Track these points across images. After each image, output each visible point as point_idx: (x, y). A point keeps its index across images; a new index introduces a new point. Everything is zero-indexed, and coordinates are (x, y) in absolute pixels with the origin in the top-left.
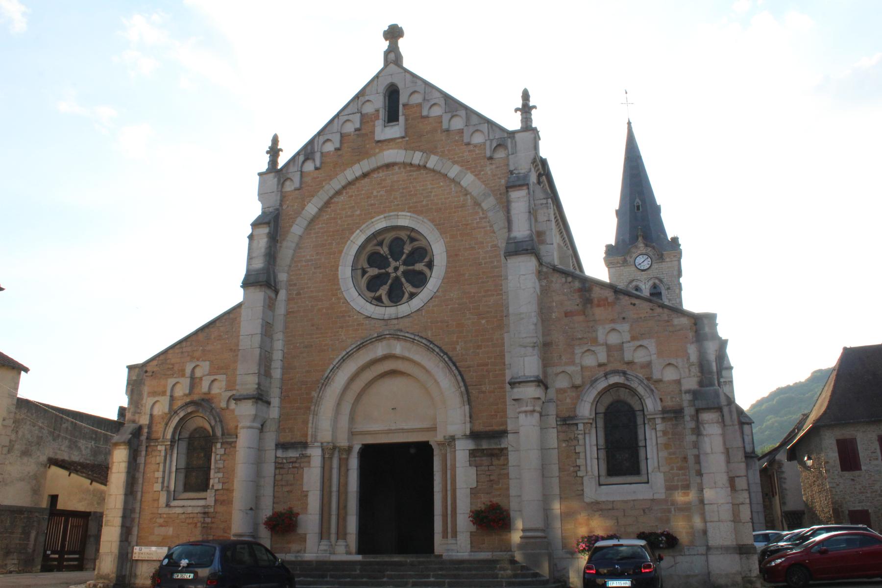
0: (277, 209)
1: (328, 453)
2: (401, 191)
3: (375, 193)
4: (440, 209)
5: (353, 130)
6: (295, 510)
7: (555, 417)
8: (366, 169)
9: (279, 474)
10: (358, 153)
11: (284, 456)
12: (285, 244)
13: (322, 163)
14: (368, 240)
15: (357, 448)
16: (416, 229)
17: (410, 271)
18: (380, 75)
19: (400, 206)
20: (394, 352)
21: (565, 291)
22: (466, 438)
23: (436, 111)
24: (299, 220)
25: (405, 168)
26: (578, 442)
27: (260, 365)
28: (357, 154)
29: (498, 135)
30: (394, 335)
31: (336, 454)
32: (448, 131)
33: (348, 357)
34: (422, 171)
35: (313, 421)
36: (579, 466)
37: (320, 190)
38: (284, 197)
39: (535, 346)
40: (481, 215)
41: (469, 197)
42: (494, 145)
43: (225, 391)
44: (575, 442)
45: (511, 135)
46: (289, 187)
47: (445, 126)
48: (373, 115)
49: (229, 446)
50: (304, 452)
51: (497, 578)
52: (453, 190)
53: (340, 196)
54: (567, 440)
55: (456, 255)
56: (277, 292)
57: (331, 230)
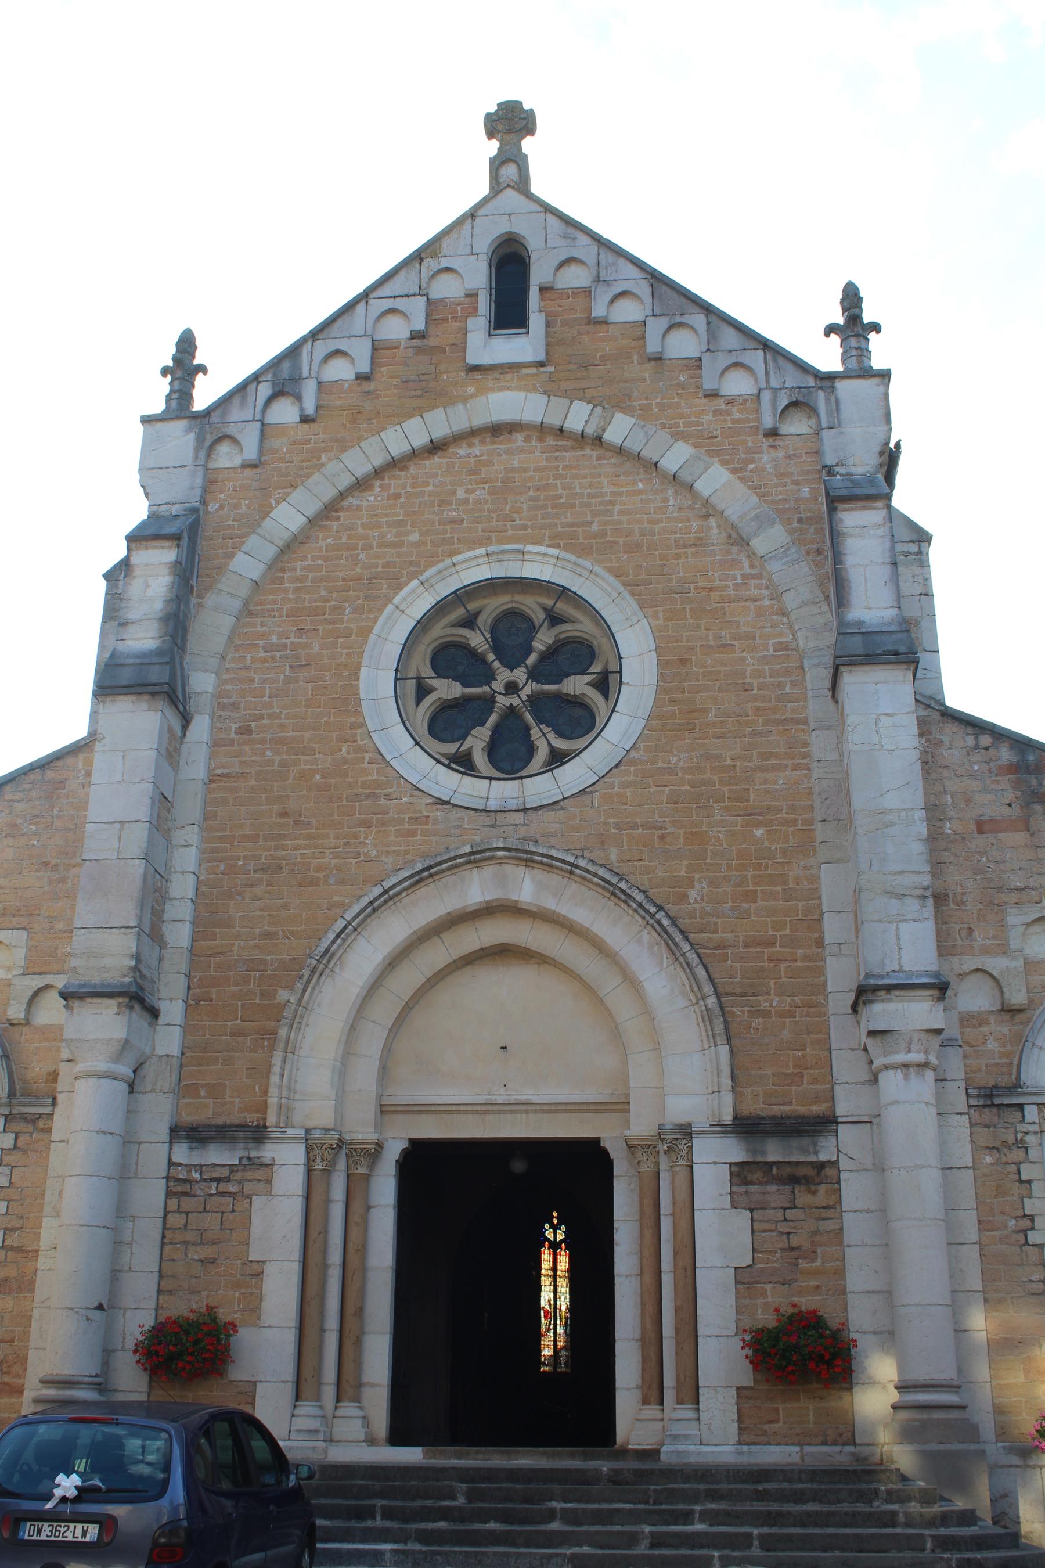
0: (194, 510)
1: (323, 1160)
2: (531, 493)
3: (461, 494)
4: (638, 546)
5: (408, 335)
6: (224, 1315)
7: (963, 1084)
8: (440, 432)
9: (178, 1211)
10: (420, 392)
11: (195, 1161)
12: (210, 600)
13: (318, 407)
14: (440, 609)
15: (394, 1151)
16: (574, 589)
17: (547, 695)
18: (480, 212)
19: (530, 531)
20: (514, 897)
21: (976, 768)
22: (724, 1132)
23: (628, 312)
24: (252, 542)
25: (541, 440)
26: (1027, 1153)
27: (142, 906)
28: (414, 393)
29: (792, 378)
30: (517, 850)
31: (341, 1164)
32: (658, 358)
33: (386, 902)
34: (588, 451)
35: (283, 1069)
36: (1032, 1218)
37: (312, 474)
38: (213, 482)
39: (926, 897)
40: (747, 570)
41: (712, 522)
42: (784, 402)
43: (23, 974)
44: (1017, 1154)
45: (827, 383)
46: (226, 458)
47: (653, 346)
48: (458, 305)
49: (31, 1128)
50: (253, 1154)
51: (894, 1526)
52: (672, 502)
53: (365, 494)
54: (997, 1149)
55: (683, 662)
56: (186, 720)
57: (341, 574)
